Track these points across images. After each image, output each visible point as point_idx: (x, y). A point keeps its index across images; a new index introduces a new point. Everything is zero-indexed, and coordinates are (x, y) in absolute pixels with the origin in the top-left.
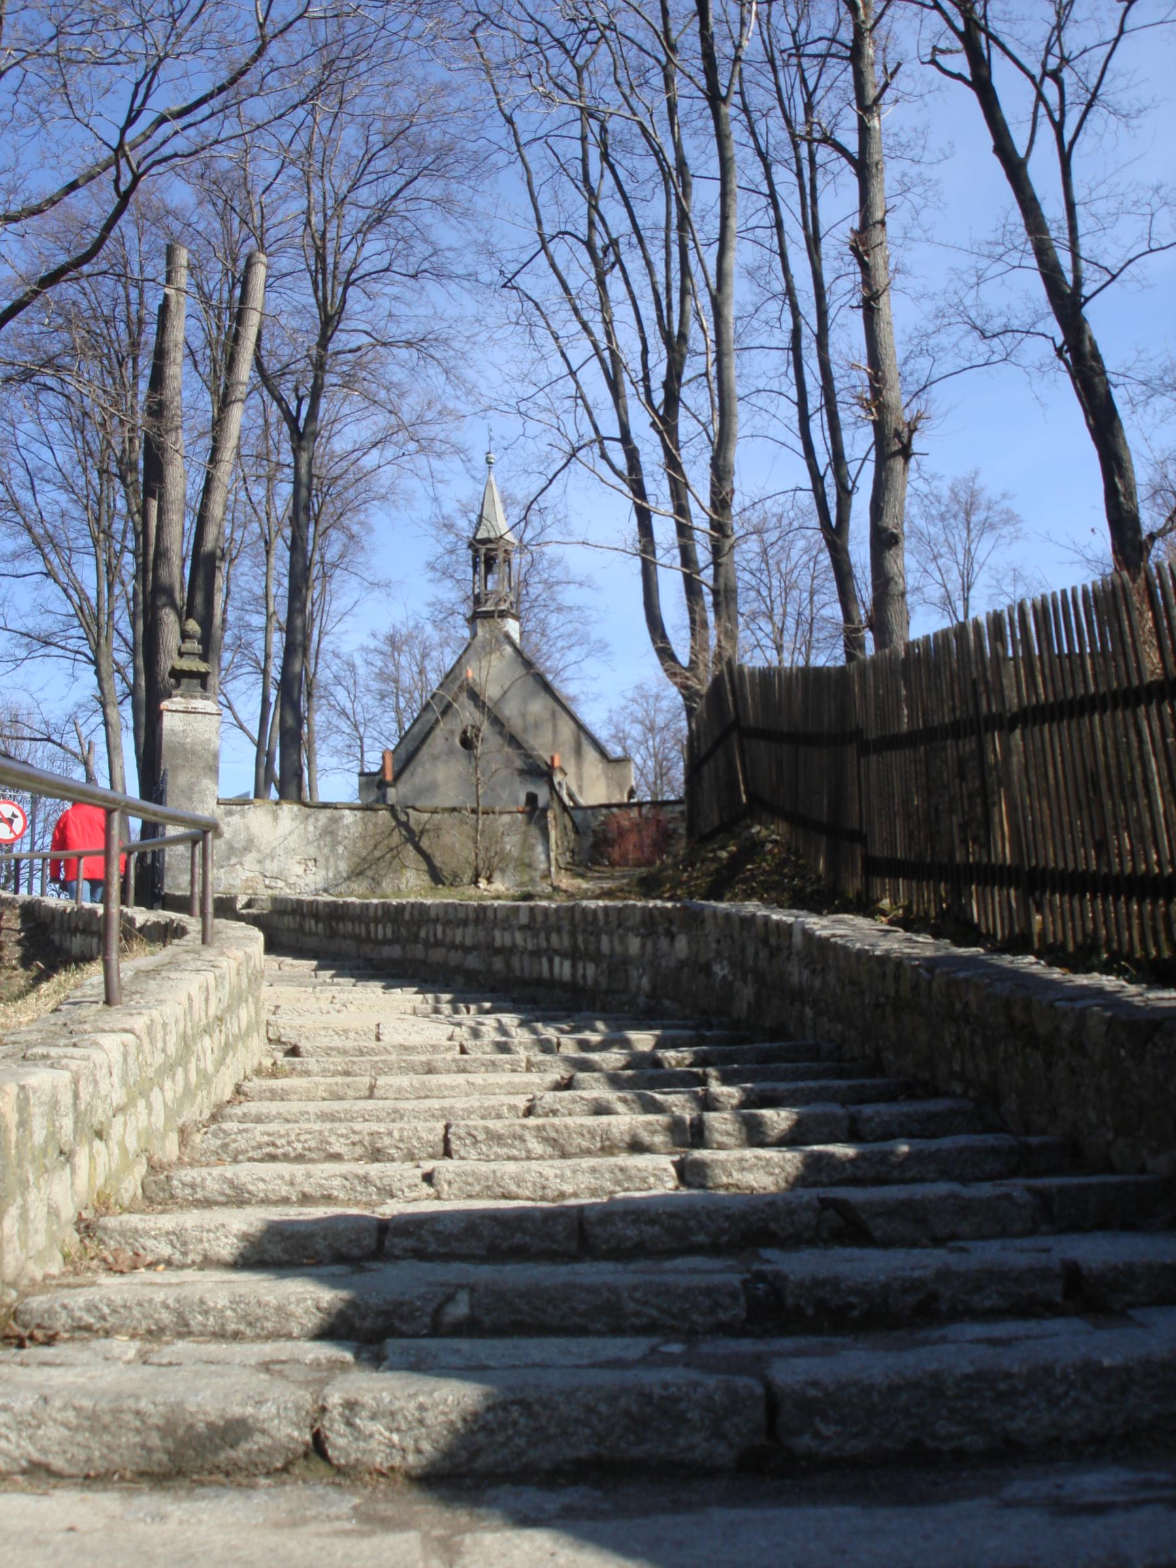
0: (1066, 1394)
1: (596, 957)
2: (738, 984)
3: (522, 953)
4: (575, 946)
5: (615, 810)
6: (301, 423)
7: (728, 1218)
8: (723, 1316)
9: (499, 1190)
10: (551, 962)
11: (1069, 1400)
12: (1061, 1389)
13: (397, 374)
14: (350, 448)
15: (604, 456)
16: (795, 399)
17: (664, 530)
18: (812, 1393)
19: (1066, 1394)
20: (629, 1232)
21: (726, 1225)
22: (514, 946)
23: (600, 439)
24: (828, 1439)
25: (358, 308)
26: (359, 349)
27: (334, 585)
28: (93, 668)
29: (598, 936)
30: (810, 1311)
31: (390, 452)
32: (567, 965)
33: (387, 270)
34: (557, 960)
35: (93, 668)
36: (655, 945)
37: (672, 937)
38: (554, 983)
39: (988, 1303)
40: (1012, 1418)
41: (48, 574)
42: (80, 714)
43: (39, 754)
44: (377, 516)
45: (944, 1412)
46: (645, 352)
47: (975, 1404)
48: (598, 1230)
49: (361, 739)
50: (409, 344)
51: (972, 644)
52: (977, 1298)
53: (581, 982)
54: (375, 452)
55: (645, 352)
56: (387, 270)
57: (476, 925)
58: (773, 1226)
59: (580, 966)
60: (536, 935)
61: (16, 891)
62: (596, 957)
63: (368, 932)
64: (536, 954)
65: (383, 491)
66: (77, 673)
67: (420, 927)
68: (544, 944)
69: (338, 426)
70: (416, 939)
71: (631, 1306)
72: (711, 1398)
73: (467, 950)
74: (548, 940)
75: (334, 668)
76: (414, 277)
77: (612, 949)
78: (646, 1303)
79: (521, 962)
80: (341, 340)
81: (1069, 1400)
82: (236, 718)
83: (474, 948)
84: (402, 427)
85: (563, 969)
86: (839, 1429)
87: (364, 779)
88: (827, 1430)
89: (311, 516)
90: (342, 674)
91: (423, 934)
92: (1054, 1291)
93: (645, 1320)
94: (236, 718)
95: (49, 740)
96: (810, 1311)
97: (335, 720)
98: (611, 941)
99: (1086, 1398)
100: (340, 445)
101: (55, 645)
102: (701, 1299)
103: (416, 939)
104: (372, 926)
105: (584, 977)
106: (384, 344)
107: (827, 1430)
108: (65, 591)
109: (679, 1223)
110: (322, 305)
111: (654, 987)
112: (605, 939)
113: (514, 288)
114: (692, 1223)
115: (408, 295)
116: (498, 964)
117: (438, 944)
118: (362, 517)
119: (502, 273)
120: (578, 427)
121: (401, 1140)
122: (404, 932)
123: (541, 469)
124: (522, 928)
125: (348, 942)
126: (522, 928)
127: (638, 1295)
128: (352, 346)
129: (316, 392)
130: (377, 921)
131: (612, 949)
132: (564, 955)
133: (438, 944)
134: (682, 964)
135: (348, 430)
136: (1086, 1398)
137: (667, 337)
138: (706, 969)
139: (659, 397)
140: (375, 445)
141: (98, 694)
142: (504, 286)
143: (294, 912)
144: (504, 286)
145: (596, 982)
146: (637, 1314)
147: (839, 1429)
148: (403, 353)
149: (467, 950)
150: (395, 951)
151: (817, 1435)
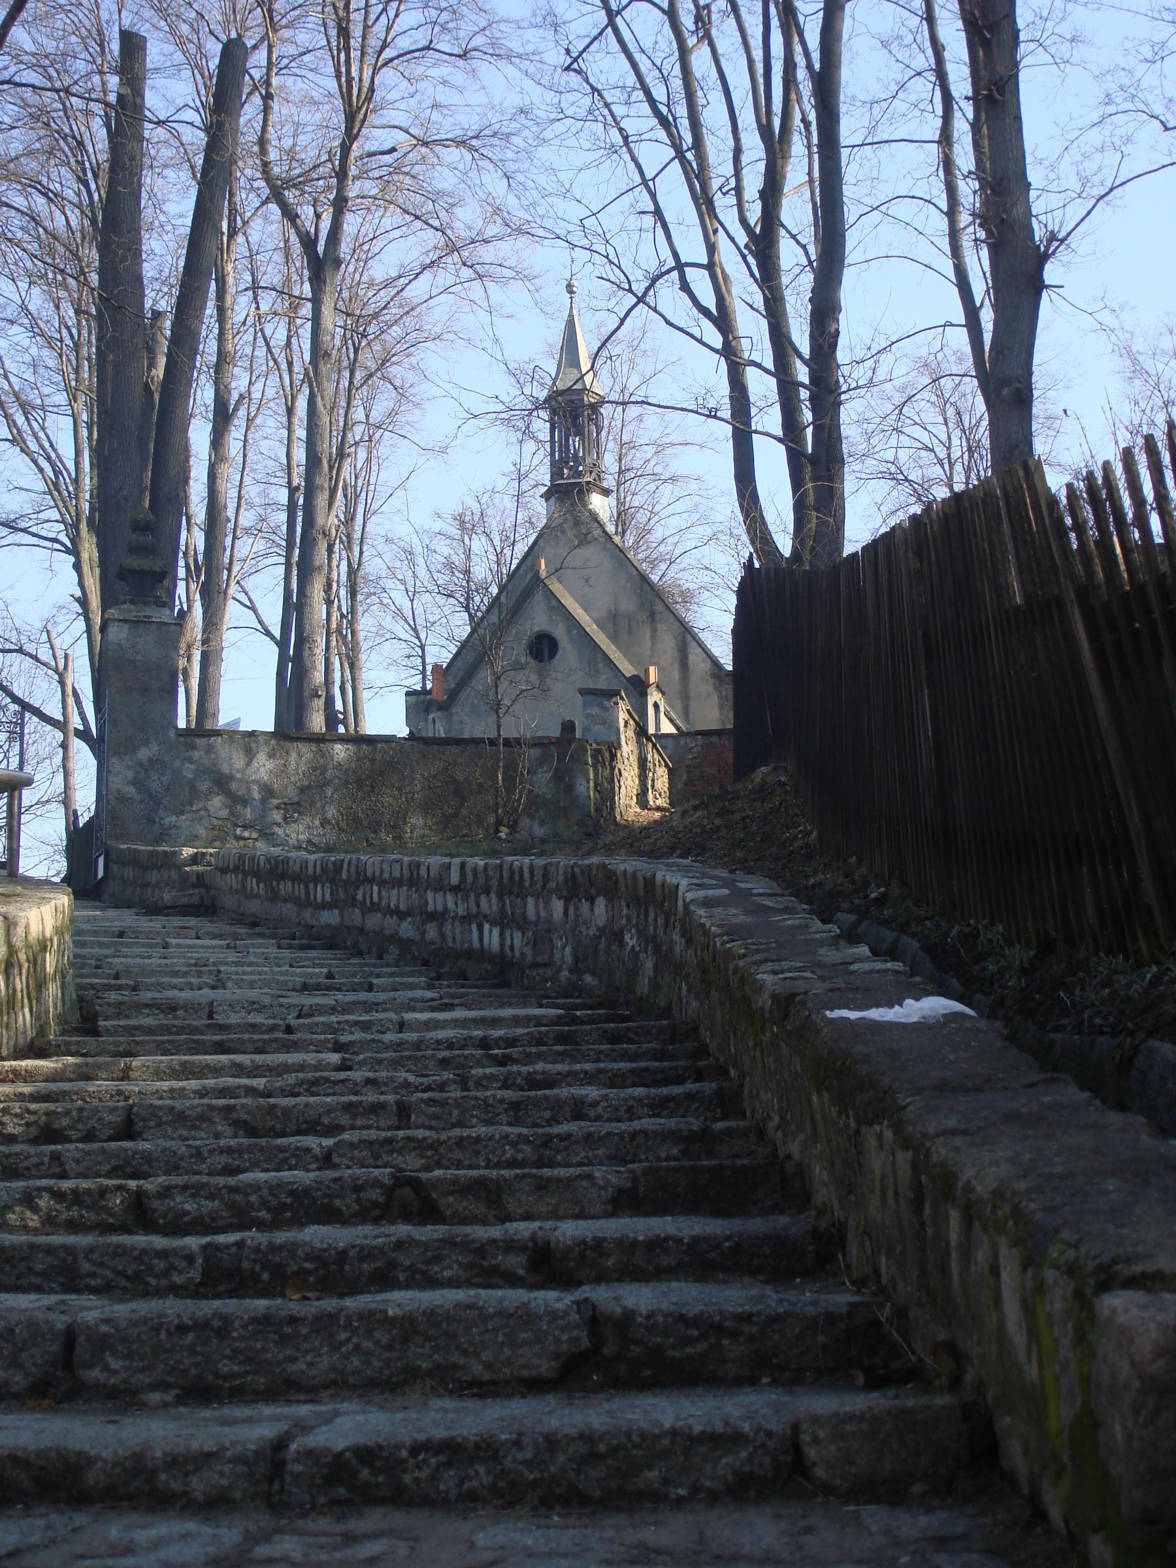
0: (348, 1340)
1: (522, 924)
2: (643, 955)
3: (454, 918)
4: (502, 910)
5: (715, 739)
6: (321, 249)
7: (291, 1193)
8: (178, 1279)
9: (129, 1170)
10: (480, 929)
11: (350, 1346)
12: (343, 1336)
13: (444, 180)
14: (394, 273)
15: (685, 287)
16: (944, 207)
17: (762, 387)
18: (104, 1328)
19: (348, 1340)
20: (187, 1206)
21: (289, 1201)
22: (446, 910)
23: (680, 266)
24: (116, 1372)
25: (393, 95)
26: (393, 150)
27: (383, 450)
28: (72, 559)
29: (524, 898)
30: (265, 1276)
31: (444, 277)
32: (496, 932)
33: (428, 48)
34: (486, 926)
35: (72, 559)
36: (577, 909)
37: (592, 900)
38: (481, 955)
39: (447, 1273)
40: (294, 1360)
41: (13, 441)
42: (60, 619)
43: (14, 669)
44: (430, 357)
45: (228, 1352)
46: (738, 151)
47: (259, 1345)
48: (156, 1204)
49: (422, 647)
50: (461, 143)
51: (295, 572)
52: (436, 1268)
53: (509, 953)
54: (426, 276)
55: (738, 151)
56: (428, 48)
57: (410, 886)
58: (338, 1202)
59: (508, 934)
60: (466, 898)
61: (463, 865)
62: (522, 924)
63: (308, 893)
64: (466, 919)
65: (438, 330)
66: (55, 566)
67: (357, 888)
68: (474, 909)
69: (379, 243)
70: (351, 901)
71: (86, 1267)
72: (13, 1331)
73: (401, 915)
74: (478, 905)
75: (386, 557)
76: (463, 56)
77: (538, 915)
78: (102, 1264)
79: (453, 930)
80: (374, 138)
81: (350, 1346)
82: (260, 622)
83: (409, 913)
84: (452, 248)
85: (492, 938)
86: (127, 1363)
87: (412, 699)
88: (115, 1364)
89: (344, 360)
90: (398, 564)
91: (359, 897)
92: (517, 1262)
93: (99, 1281)
94: (260, 622)
95: (20, 651)
96: (265, 1276)
97: (388, 622)
98: (537, 905)
99: (367, 1344)
100: (380, 270)
101: (25, 530)
102: (156, 1261)
103: (351, 901)
104: (311, 886)
105: (512, 948)
106: (426, 144)
107: (115, 1364)
108: (35, 462)
109: (238, 1197)
110: (346, 96)
111: (576, 960)
112: (530, 901)
113: (579, 72)
114: (253, 1198)
115: (459, 78)
116: (432, 932)
117: (374, 908)
118: (413, 360)
119: (568, 52)
120: (644, 254)
121: (80, 1120)
122: (342, 894)
123: (611, 305)
124: (455, 889)
125: (289, 905)
126: (455, 889)
127: (95, 1256)
128: (387, 146)
129: (340, 205)
130: (316, 880)
131: (538, 915)
132: (493, 923)
133: (374, 908)
134: (602, 930)
135: (386, 248)
136: (367, 1344)
137: (765, 131)
138: (619, 937)
139: (754, 213)
140: (424, 268)
141: (79, 594)
142: (568, 69)
143: (236, 869)
144: (568, 69)
145: (522, 954)
146: (92, 1275)
147: (127, 1363)
148: (453, 155)
149: (401, 915)
150: (331, 917)
151: (106, 1368)
